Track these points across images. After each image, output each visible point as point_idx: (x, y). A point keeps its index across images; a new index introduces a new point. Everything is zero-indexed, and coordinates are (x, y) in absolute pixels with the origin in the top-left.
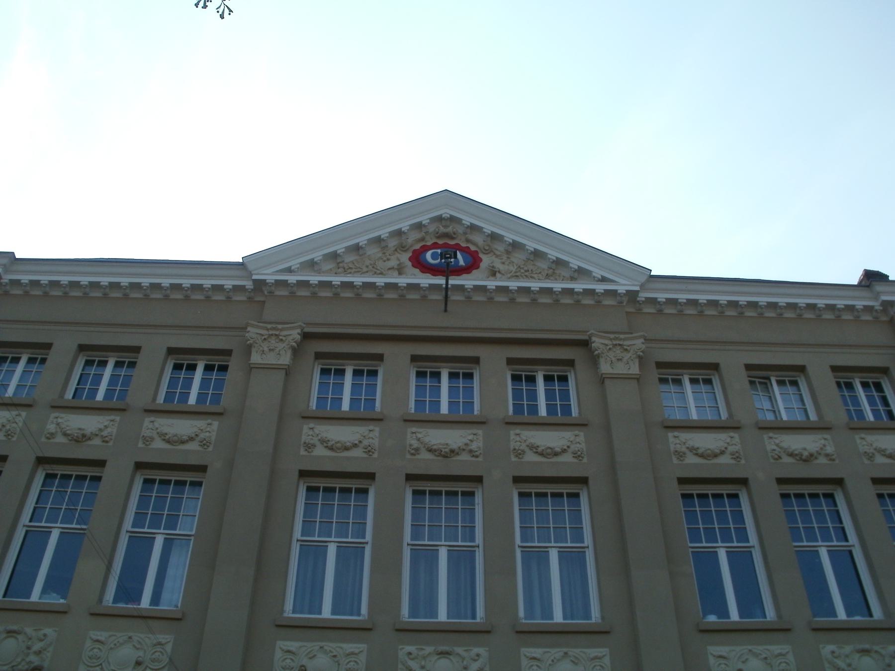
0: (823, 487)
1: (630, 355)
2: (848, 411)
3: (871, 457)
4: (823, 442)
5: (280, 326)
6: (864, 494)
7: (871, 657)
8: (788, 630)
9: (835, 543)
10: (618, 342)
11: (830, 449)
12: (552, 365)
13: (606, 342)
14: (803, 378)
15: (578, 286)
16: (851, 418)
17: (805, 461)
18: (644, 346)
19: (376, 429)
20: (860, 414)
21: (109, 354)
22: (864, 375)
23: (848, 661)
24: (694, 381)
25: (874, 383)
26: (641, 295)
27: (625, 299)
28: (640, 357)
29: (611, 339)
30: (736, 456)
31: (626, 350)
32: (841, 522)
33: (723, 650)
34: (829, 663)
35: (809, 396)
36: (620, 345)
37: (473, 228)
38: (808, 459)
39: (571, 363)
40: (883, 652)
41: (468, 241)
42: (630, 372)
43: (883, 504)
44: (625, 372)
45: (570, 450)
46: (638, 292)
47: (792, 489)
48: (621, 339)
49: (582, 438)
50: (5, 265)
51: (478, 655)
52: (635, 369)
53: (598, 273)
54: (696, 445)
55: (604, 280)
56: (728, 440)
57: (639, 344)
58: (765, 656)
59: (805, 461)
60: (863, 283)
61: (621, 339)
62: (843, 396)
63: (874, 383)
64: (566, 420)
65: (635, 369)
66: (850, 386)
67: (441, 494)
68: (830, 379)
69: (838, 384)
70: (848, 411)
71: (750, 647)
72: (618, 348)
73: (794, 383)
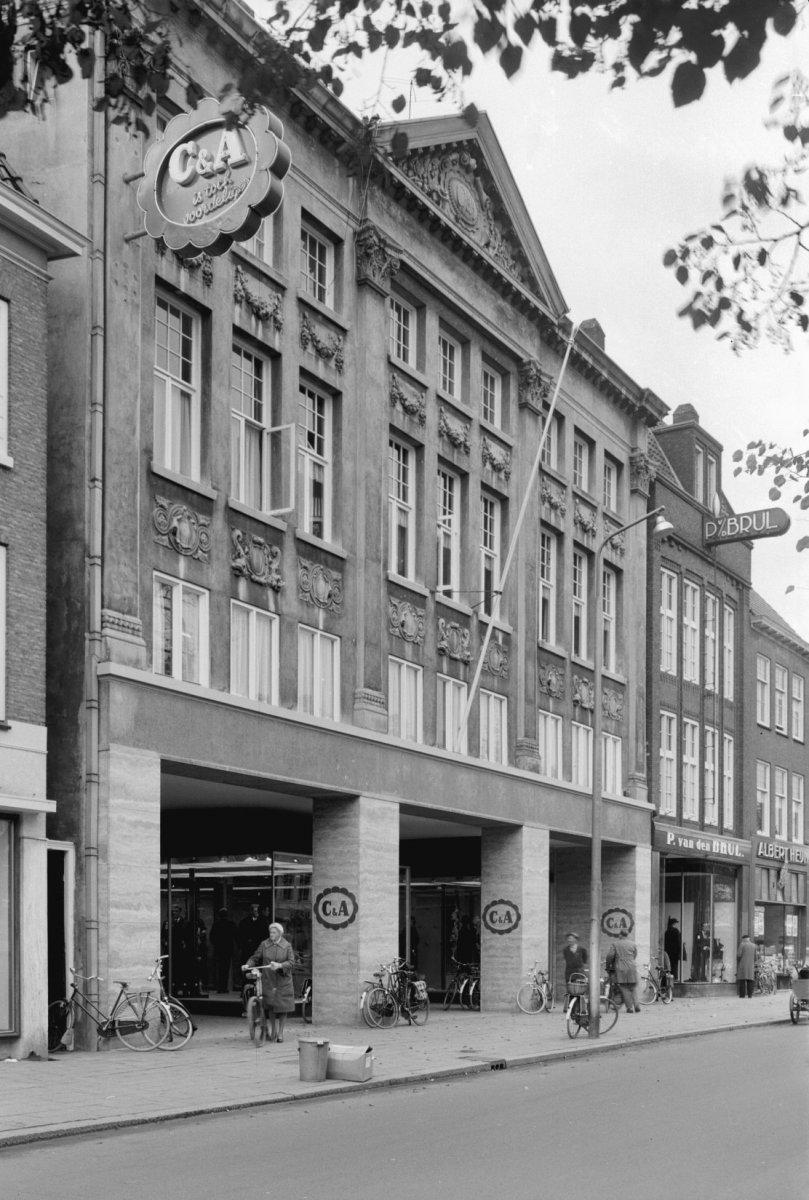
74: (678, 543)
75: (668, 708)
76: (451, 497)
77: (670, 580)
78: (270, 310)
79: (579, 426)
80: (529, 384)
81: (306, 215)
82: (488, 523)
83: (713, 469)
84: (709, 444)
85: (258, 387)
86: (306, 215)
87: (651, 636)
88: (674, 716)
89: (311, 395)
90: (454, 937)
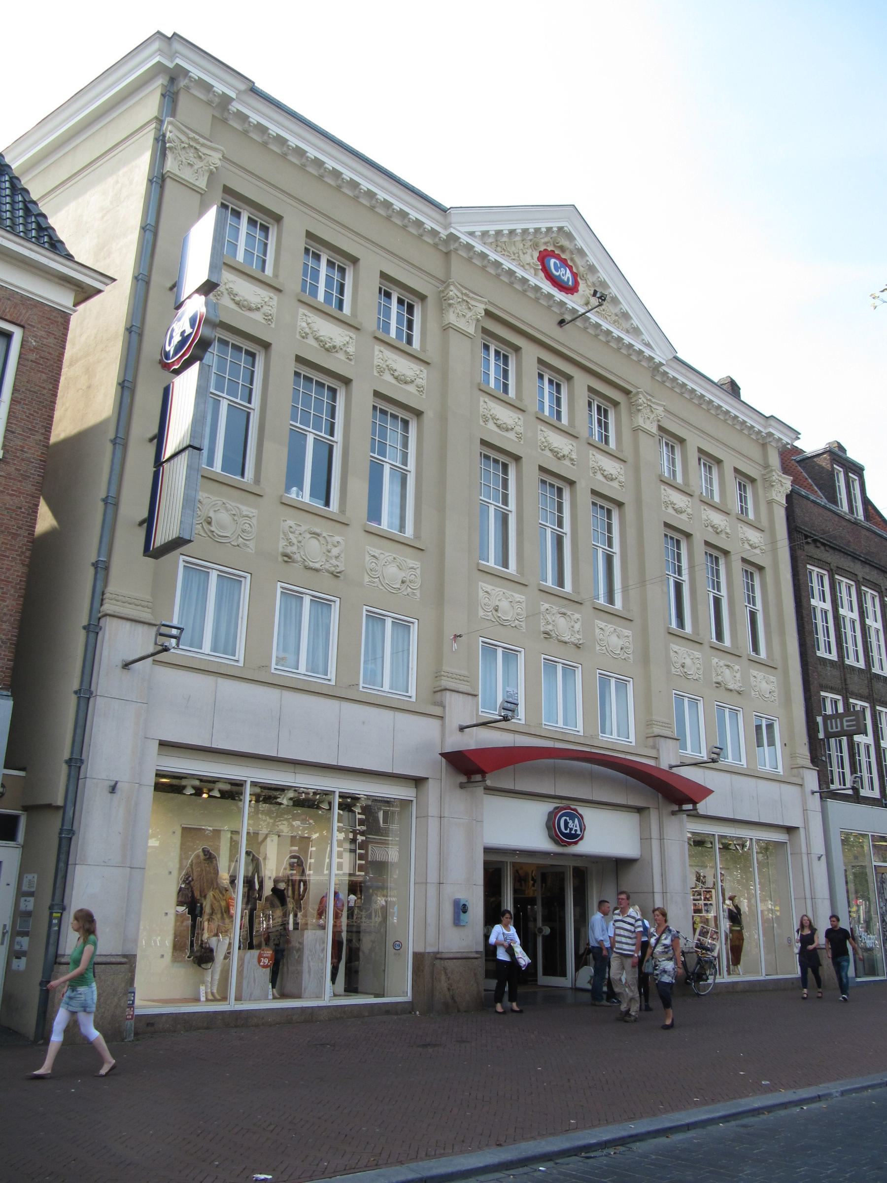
0: (330, 379)
1: (201, 164)
2: (305, 281)
3: (381, 372)
4: (347, 339)
5: (471, 295)
6: (283, 367)
7: (319, 540)
8: (347, 525)
9: (322, 434)
10: (195, 145)
11: (351, 349)
12: (265, 214)
13: (184, 138)
14: (276, 227)
15: (627, 339)
16: (304, 290)
17: (327, 350)
18: (219, 163)
19: (685, 498)
20: (387, 329)
21: (546, 370)
22: (403, 292)
23: (300, 538)
24: (252, 222)
25: (557, 383)
26: (234, 104)
27: (217, 100)
28: (211, 173)
29: (462, 294)
30: (268, 318)
31: (200, 157)
32: (251, 384)
33: (489, 588)
34: (284, 533)
35: (351, 290)
36: (196, 149)
37: (581, 252)
38: (331, 350)
39: (616, 404)
40: (328, 539)
41: (572, 260)
42: (197, 183)
43: (296, 383)
44: (191, 181)
45: (262, 310)
46: (233, 99)
47: (305, 371)
48: (199, 143)
49: (424, 375)
50: (159, 50)
51: (338, 542)
52: (202, 183)
53: (646, 337)
54: (235, 290)
55: (648, 345)
56: (266, 299)
57: (215, 158)
58: (234, 512)
59: (327, 350)
60: (724, 387)
61: (199, 143)
62: (306, 265)
63: (557, 383)
64: (407, 348)
65: (202, 183)
66: (388, 295)
67: (228, 346)
68: (375, 283)
69: (307, 251)
70: (305, 281)
71: (225, 501)
72: (193, 150)
73: (265, 229)
74: (824, 544)
75: (832, 690)
76: (753, 585)
77: (849, 588)
78: (566, 452)
79: (228, 185)
80: (773, 486)
81: (736, 470)
82: (751, 588)
83: (857, 485)
84: (847, 464)
85: (610, 526)
86: (736, 470)
87: (803, 624)
88: (866, 704)
89: (602, 507)
90: (291, 916)
